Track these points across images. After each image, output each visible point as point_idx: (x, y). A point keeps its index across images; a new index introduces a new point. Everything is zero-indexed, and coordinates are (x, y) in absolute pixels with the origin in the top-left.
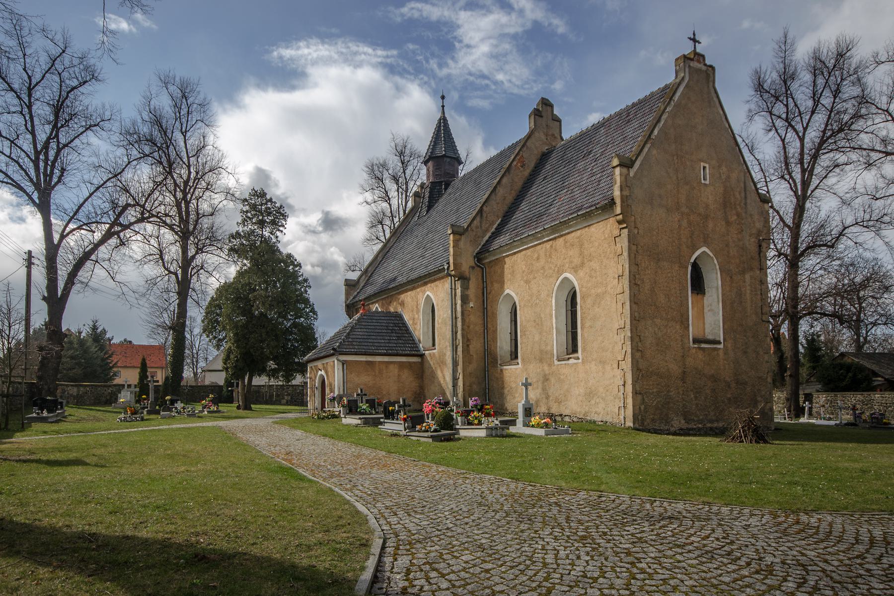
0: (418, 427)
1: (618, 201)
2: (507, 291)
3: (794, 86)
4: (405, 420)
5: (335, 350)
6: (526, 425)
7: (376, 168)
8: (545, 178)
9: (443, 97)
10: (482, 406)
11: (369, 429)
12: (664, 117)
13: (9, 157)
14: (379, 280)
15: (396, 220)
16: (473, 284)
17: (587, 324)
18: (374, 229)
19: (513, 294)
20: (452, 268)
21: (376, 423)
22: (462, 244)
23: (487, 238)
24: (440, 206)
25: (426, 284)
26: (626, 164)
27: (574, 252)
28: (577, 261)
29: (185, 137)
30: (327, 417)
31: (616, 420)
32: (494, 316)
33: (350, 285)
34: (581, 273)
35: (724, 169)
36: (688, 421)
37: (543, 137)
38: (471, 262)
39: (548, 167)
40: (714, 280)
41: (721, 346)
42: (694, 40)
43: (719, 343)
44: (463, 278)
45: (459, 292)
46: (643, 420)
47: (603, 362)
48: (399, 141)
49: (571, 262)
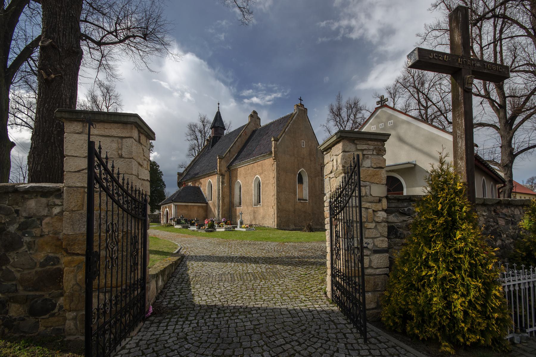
0: (201, 228)
1: (273, 152)
2: (238, 180)
3: (342, 112)
4: (197, 225)
5: (172, 200)
6: (241, 227)
7: (192, 126)
8: (253, 140)
9: (219, 104)
10: (226, 221)
11: (184, 230)
12: (290, 125)
13: (27, 115)
14: (192, 173)
15: (200, 148)
16: (226, 177)
17: (264, 193)
18: (191, 151)
19: (240, 182)
20: (218, 171)
21: (187, 227)
22: (222, 162)
23: (232, 160)
24: (216, 146)
25: (209, 176)
26: (276, 140)
27: (260, 168)
28: (261, 171)
29: (108, 109)
30: (169, 226)
31: (271, 226)
32: (234, 189)
33: (180, 174)
34: (262, 176)
35: (310, 143)
36: (295, 226)
37: (254, 125)
38: (226, 169)
39: (254, 136)
40: (306, 179)
41: (308, 201)
42: (301, 100)
43: (307, 200)
44: (222, 175)
45: (221, 180)
46: (280, 226)
47: (268, 206)
48: (202, 117)
49: (259, 172)
